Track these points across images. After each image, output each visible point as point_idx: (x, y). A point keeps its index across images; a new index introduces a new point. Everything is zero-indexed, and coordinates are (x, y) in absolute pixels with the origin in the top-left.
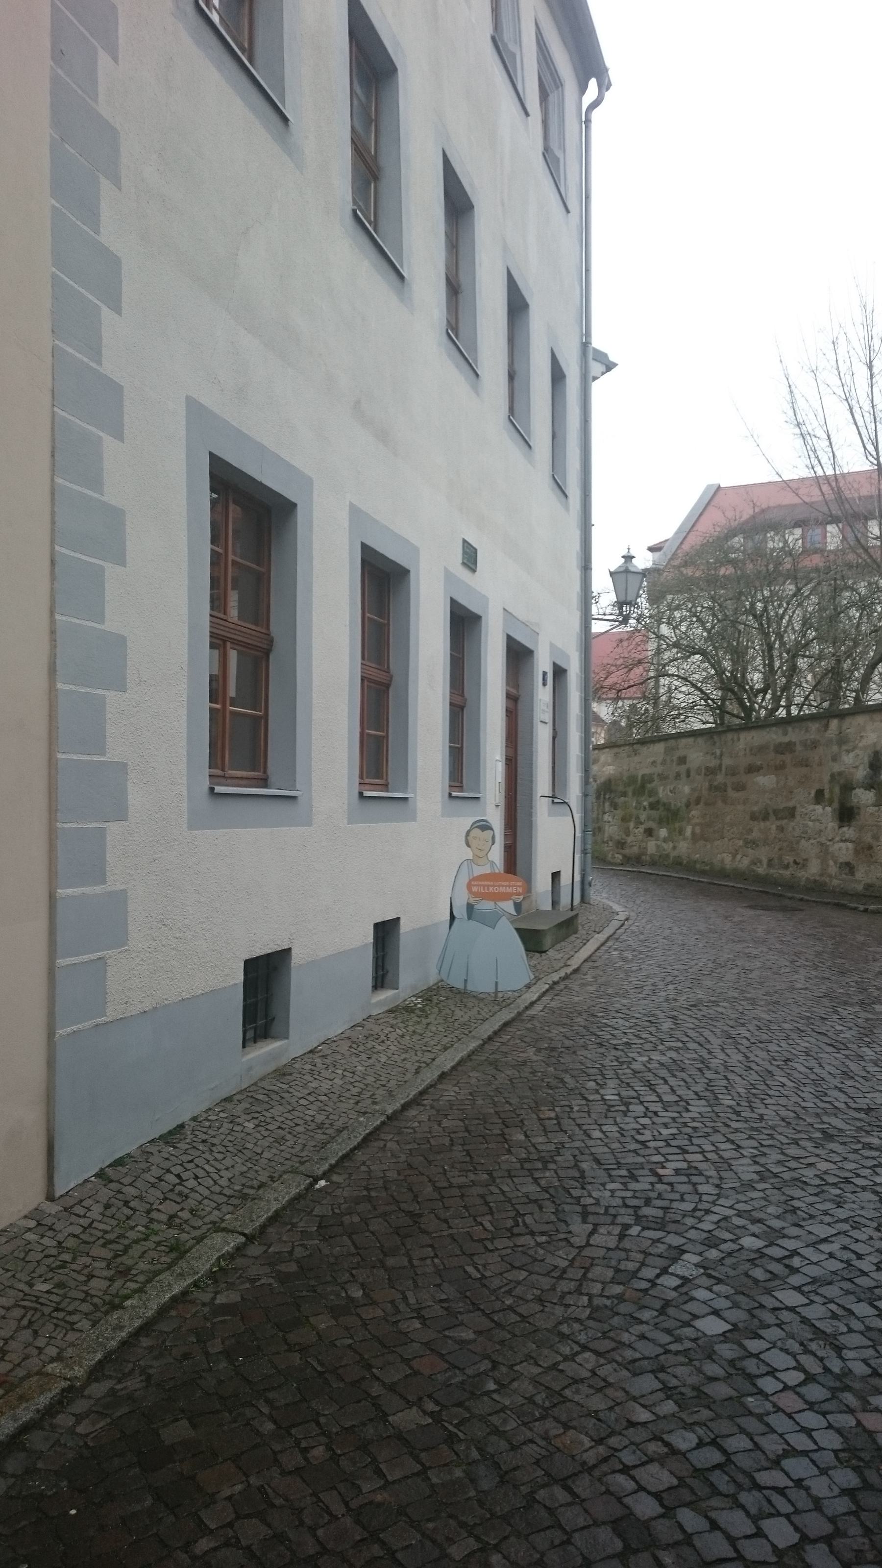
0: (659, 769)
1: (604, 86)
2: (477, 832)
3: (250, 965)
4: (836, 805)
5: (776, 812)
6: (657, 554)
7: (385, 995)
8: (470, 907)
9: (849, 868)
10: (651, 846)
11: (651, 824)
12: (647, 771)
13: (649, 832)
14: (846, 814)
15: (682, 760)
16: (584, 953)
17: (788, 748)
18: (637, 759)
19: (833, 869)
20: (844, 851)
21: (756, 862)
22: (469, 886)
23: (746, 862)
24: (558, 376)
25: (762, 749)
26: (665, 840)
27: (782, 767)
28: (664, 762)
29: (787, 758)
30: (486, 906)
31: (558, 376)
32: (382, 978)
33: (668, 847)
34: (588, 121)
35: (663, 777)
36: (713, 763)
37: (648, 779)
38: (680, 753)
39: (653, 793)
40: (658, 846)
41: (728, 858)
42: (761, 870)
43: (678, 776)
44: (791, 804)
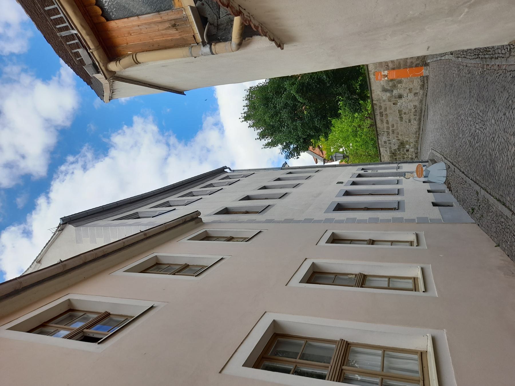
0: (388, 149)
1: (226, 168)
2: (406, 177)
3: (434, 206)
4: (397, 99)
5: (400, 115)
6: (318, 160)
7: (446, 191)
8: (425, 177)
9: (416, 94)
10: (412, 150)
11: (405, 150)
12: (389, 153)
13: (408, 151)
14: (400, 97)
15: (385, 142)
16: (439, 155)
17: (381, 113)
18: (385, 156)
19: (417, 98)
20: (411, 96)
21: (415, 119)
22: (420, 177)
23: (415, 122)
24: (290, 173)
25: (382, 121)
26: (410, 146)
27: (386, 115)
28: (386, 148)
29: (384, 113)
30: (424, 173)
31: (290, 173)
32: (449, 205)
33: (412, 145)
34: (233, 171)
35: (390, 148)
36: (386, 133)
37: (391, 152)
38: (383, 143)
39: (395, 150)
40: (412, 148)
41: (415, 127)
42: (418, 118)
43: (390, 143)
44: (398, 111)
